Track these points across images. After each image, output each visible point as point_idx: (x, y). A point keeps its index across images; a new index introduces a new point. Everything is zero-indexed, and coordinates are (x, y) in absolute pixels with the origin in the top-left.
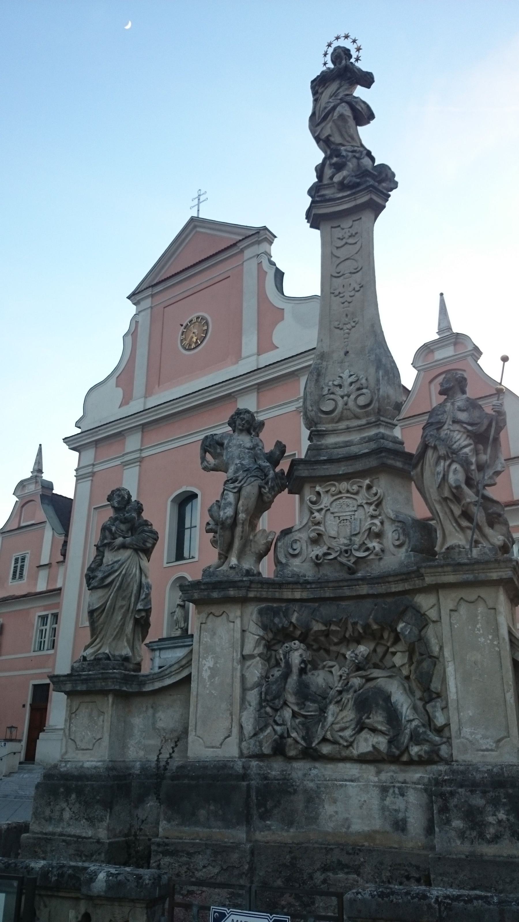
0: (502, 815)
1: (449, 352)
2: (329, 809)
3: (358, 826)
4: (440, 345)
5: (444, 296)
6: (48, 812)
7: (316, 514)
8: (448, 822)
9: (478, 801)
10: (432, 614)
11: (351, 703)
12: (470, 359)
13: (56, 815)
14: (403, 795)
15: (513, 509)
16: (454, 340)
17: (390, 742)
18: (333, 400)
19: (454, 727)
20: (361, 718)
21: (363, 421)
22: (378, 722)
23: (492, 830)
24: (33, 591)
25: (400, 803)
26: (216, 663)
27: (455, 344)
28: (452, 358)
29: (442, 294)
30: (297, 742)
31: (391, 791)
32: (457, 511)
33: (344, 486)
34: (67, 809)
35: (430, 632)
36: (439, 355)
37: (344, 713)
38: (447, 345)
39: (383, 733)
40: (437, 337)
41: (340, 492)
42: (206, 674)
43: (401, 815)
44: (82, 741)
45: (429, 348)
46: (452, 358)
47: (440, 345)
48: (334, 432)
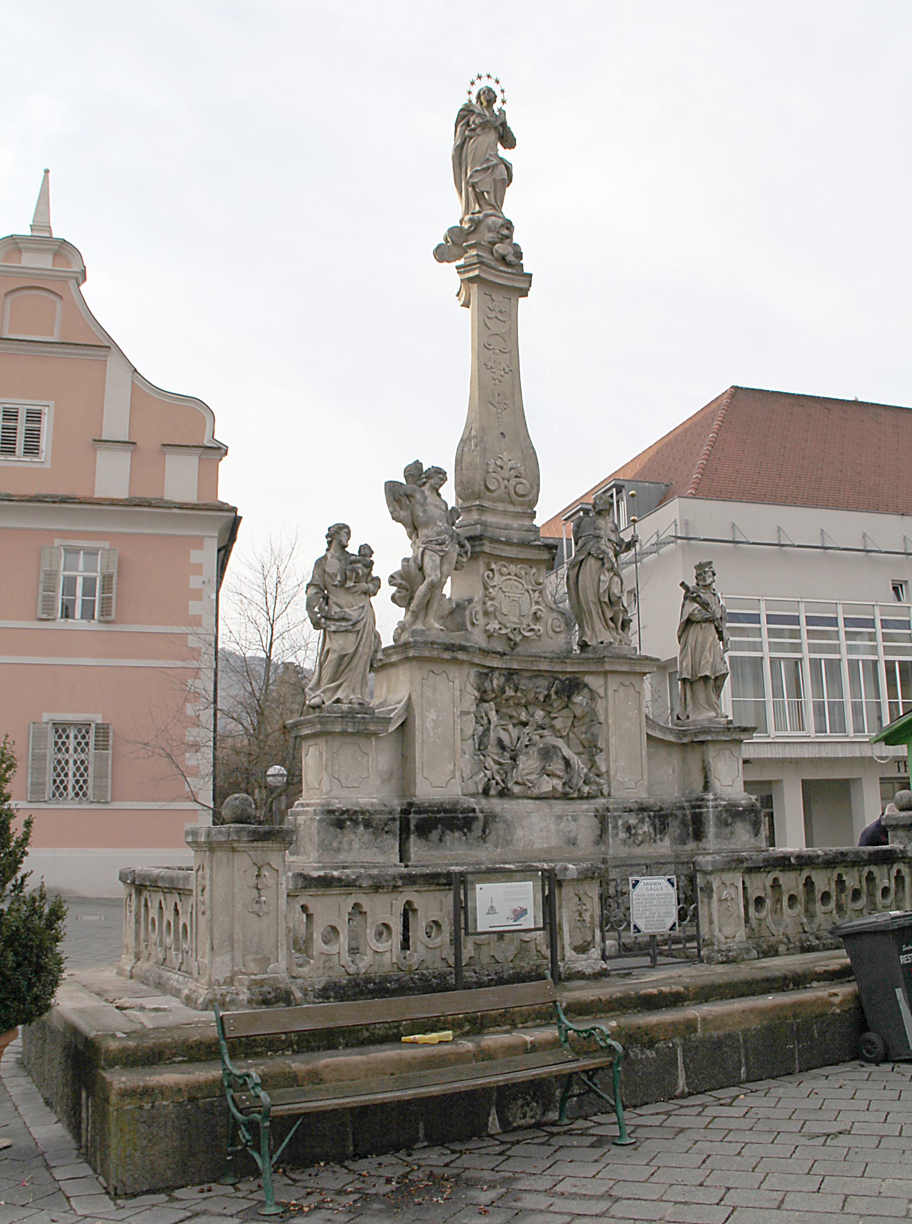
0: (646, 829)
1: (44, 262)
2: (520, 833)
3: (538, 846)
4: (32, 246)
5: (50, 175)
6: (335, 845)
7: (491, 590)
8: (617, 834)
9: (633, 821)
10: (601, 692)
11: (536, 754)
12: (72, 284)
13: (345, 846)
14: (574, 820)
15: (113, 510)
16: (56, 247)
17: (564, 784)
18: (515, 488)
19: (612, 773)
20: (544, 766)
21: (519, 509)
22: (557, 769)
23: (640, 838)
24: (81, 493)
25: (573, 826)
26: (438, 716)
27: (56, 254)
28: (47, 273)
29: (47, 171)
30: (497, 783)
31: (565, 818)
32: (609, 615)
33: (512, 568)
34: (357, 839)
35: (600, 705)
36: (29, 260)
37: (531, 762)
38: (46, 250)
39: (559, 777)
40: (28, 232)
41: (509, 574)
42: (429, 725)
43: (572, 835)
44: (347, 779)
45: (17, 243)
46: (47, 273)
47: (32, 246)
48: (494, 511)
